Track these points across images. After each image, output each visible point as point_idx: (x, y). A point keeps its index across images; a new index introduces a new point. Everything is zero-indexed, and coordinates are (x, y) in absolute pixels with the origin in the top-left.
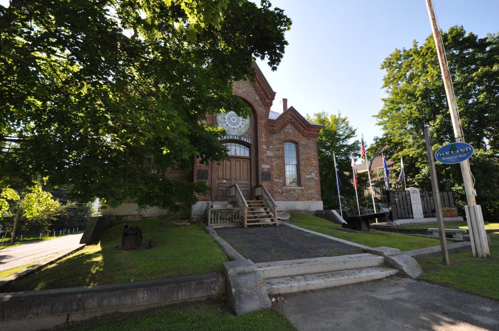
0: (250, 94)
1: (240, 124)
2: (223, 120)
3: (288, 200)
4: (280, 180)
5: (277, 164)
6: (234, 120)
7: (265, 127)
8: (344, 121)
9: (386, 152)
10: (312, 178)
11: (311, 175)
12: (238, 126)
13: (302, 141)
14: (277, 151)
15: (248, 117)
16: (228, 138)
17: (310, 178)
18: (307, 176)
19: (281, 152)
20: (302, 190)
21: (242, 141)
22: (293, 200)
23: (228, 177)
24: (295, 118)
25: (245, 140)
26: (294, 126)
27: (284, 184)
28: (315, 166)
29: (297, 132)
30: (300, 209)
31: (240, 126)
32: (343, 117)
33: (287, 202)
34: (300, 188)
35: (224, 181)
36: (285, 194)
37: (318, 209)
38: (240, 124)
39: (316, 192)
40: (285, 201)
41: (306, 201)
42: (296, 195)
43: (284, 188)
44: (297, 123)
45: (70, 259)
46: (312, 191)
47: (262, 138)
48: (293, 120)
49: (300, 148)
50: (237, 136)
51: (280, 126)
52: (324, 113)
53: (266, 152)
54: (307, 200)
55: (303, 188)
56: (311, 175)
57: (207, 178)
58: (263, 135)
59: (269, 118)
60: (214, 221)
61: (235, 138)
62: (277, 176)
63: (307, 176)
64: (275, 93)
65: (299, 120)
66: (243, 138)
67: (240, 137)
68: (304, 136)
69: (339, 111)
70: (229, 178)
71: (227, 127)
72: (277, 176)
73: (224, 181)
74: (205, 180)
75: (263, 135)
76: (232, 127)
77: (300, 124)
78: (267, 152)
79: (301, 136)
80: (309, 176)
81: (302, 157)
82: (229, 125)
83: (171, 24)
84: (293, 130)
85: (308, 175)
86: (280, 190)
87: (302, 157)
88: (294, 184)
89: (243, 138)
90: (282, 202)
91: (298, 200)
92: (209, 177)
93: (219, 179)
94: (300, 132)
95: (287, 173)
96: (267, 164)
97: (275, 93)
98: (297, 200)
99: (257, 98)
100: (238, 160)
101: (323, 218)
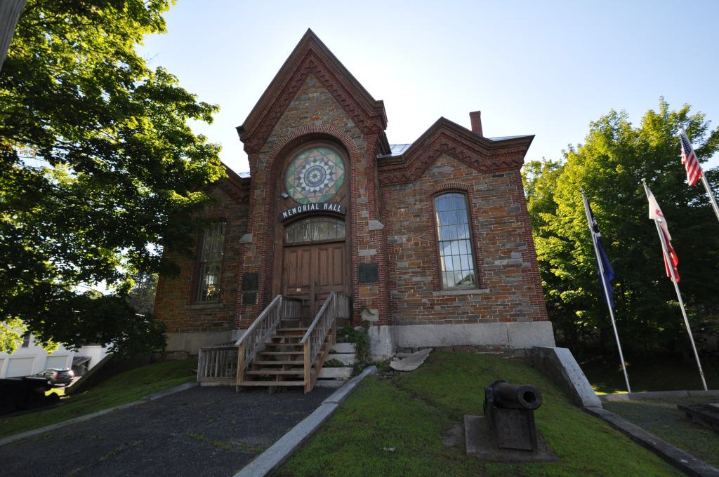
0: (336, 122)
1: (326, 182)
2: (297, 181)
3: (447, 322)
4: (424, 279)
5: (417, 244)
6: (315, 176)
7: (366, 174)
8: (682, 117)
9: (45, 52)
10: (512, 266)
11: (510, 257)
12: (322, 186)
13: (478, 184)
14: (414, 216)
15: (17, 147)
16: (300, 211)
17: (505, 267)
18: (497, 263)
19: (425, 218)
20: (486, 297)
21: (325, 211)
22: (460, 322)
23: (305, 282)
24: (454, 140)
25: (331, 207)
26: (455, 156)
27: (438, 284)
28: (519, 235)
29: (463, 168)
30: (482, 343)
31: (326, 185)
32: (675, 108)
33: (444, 326)
34: (479, 291)
35: (299, 290)
36: (438, 308)
37: (536, 344)
38: (326, 182)
39: (527, 299)
40: (439, 323)
41: (499, 323)
42: (469, 309)
43: (435, 294)
44: (459, 149)
45: (103, 409)
46: (517, 298)
47: (360, 196)
48: (451, 145)
49: (474, 201)
50: (315, 204)
51: (418, 164)
52: (615, 113)
53: (367, 224)
54: (501, 320)
55: (488, 291)
56: (510, 257)
57: (257, 288)
58: (362, 191)
59: (396, 152)
60: (219, 375)
61: (313, 207)
62: (419, 270)
63: (497, 263)
64: (381, 102)
65: (464, 141)
66: (326, 206)
67: (321, 205)
68: (480, 171)
69: (662, 98)
70: (307, 283)
71: (304, 192)
72: (419, 270)
73: (299, 290)
74: (253, 292)
75: (362, 191)
76: (312, 189)
77: (469, 148)
78: (369, 221)
79: (475, 173)
80: (505, 262)
81: (481, 219)
82: (307, 188)
83: (25, 52)
84: (453, 166)
85: (501, 258)
86: (424, 300)
87: (481, 219)
88: (468, 282)
89: (326, 206)
90: (430, 326)
91: (475, 321)
92: (261, 286)
93: (289, 287)
94: (470, 165)
95: (447, 264)
96: (371, 247)
97: (381, 102)
98: (472, 320)
99: (351, 124)
100: (323, 247)
101: (273, 442)
